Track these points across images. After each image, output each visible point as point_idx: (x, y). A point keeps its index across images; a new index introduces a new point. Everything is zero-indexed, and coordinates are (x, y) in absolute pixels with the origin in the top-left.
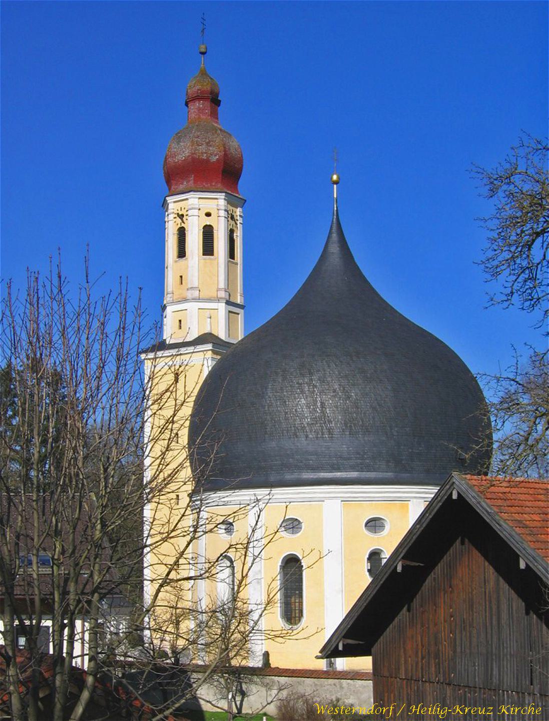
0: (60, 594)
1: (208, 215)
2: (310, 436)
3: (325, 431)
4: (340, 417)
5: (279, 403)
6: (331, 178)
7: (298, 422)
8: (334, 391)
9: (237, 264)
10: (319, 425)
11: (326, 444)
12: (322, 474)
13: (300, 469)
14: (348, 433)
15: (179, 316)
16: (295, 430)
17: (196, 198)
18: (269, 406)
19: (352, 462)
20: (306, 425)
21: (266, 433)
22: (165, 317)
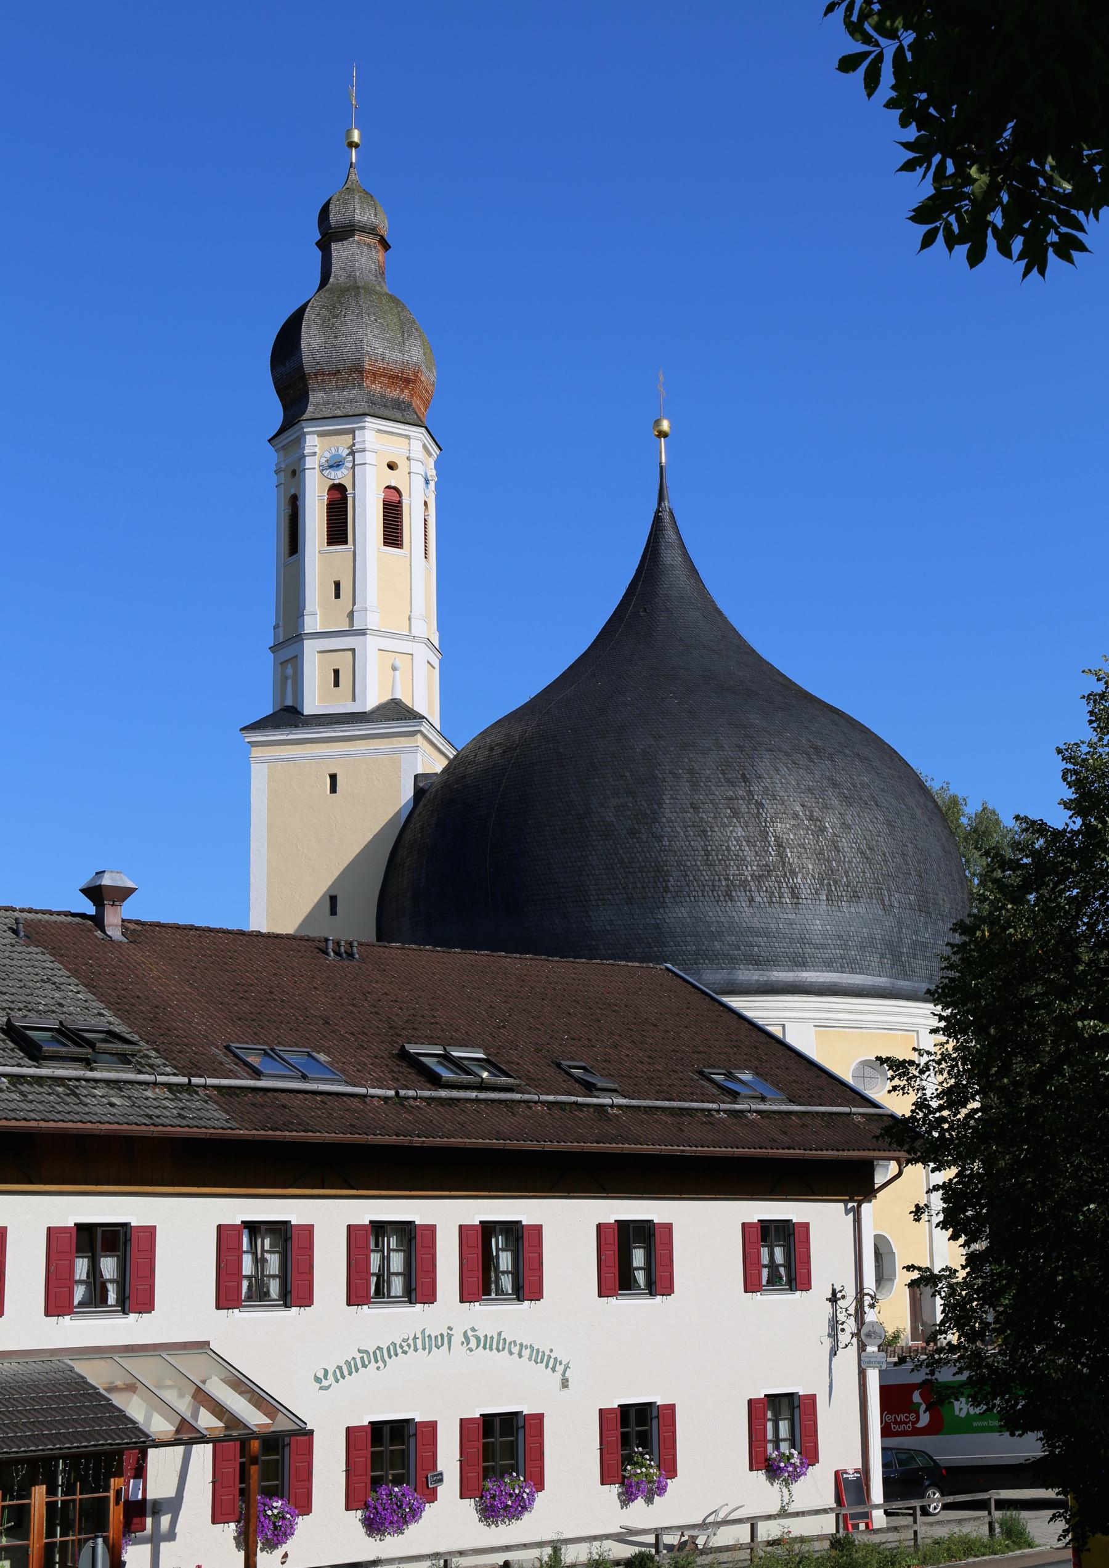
2: (758, 899)
3: (785, 890)
4: (810, 867)
7: (733, 870)
8: (796, 816)
11: (785, 916)
12: (775, 973)
13: (801, 963)
19: (827, 954)
21: (666, 890)
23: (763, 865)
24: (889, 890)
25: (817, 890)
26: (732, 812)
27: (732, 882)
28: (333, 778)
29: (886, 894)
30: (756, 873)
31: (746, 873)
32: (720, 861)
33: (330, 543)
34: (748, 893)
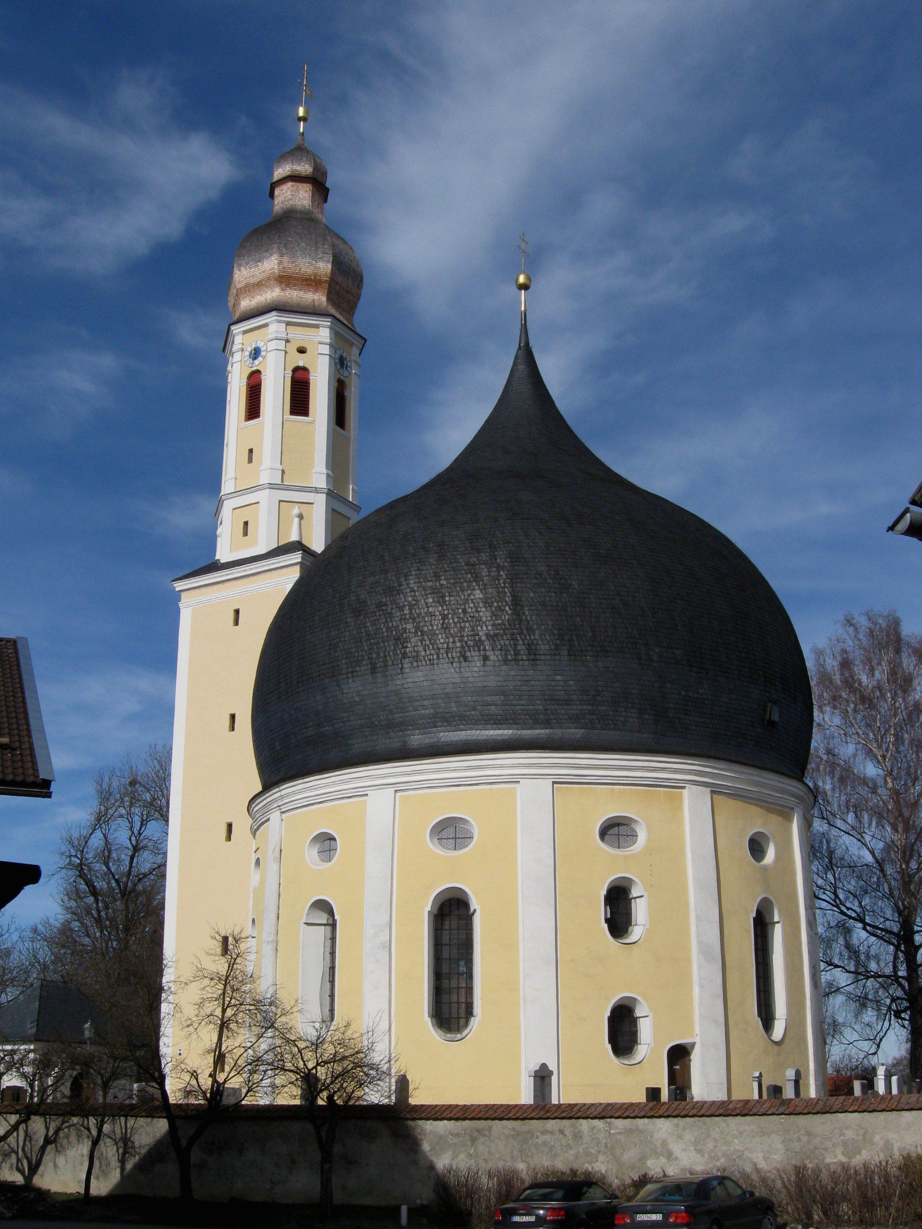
1: (302, 351)
2: (492, 658)
5: (431, 600)
6: (517, 279)
9: (348, 439)
14: (565, 653)
15: (245, 515)
16: (462, 647)
17: (283, 322)
18: (411, 607)
20: (484, 638)
21: (404, 656)
22: (221, 524)
23: (499, 624)
26: (472, 577)
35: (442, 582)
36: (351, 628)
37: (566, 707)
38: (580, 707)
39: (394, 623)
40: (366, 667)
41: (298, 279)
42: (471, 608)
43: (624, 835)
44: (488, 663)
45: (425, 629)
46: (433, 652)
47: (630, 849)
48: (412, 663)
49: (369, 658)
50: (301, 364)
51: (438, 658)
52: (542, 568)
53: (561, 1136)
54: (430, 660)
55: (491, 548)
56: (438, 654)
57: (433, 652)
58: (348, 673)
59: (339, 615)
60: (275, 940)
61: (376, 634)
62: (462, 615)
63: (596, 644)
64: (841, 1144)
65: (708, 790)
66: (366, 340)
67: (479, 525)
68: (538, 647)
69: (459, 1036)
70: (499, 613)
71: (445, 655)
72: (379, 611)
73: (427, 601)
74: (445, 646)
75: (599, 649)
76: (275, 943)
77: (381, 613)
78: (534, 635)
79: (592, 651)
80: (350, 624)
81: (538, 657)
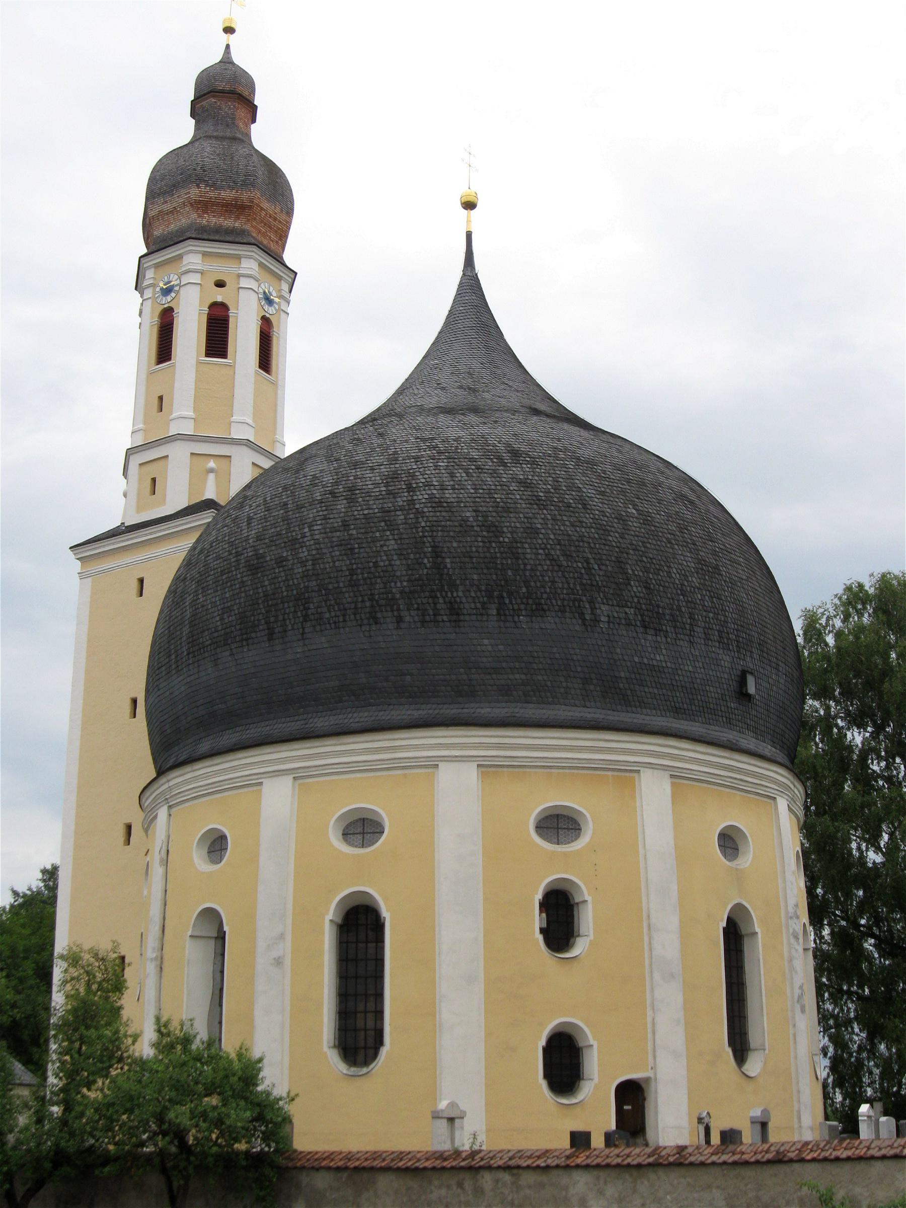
0: (807, 795)
1: (220, 284)
2: (407, 619)
10: (427, 594)
14: (495, 612)
15: (152, 471)
20: (398, 596)
23: (416, 580)
24: (591, 602)
25: (483, 604)
26: (386, 525)
27: (377, 601)
28: (141, 581)
29: (587, 606)
30: (407, 590)
31: (394, 590)
32: (365, 579)
33: (208, 354)
34: (396, 613)
35: (351, 532)
36: (247, 588)
37: (494, 676)
38: (511, 677)
39: (295, 581)
40: (263, 633)
41: (217, 204)
42: (384, 561)
43: (564, 828)
44: (403, 625)
45: (330, 587)
46: (338, 613)
47: (570, 845)
48: (314, 626)
49: (266, 623)
50: (219, 299)
51: (345, 621)
52: (468, 514)
53: (459, 1190)
54: (335, 623)
55: (408, 492)
56: (344, 616)
57: (338, 613)
58: (242, 641)
59: (234, 573)
60: (159, 956)
61: (274, 594)
62: (373, 570)
63: (530, 601)
64: (796, 1201)
65: (667, 774)
66: (296, 274)
67: (397, 466)
68: (462, 606)
69: (365, 1070)
70: (417, 567)
71: (352, 617)
72: (279, 567)
73: (333, 554)
74: (353, 606)
75: (534, 607)
76: (159, 959)
77: (281, 569)
78: (457, 591)
79: (526, 610)
80: (246, 584)
81: (462, 617)
